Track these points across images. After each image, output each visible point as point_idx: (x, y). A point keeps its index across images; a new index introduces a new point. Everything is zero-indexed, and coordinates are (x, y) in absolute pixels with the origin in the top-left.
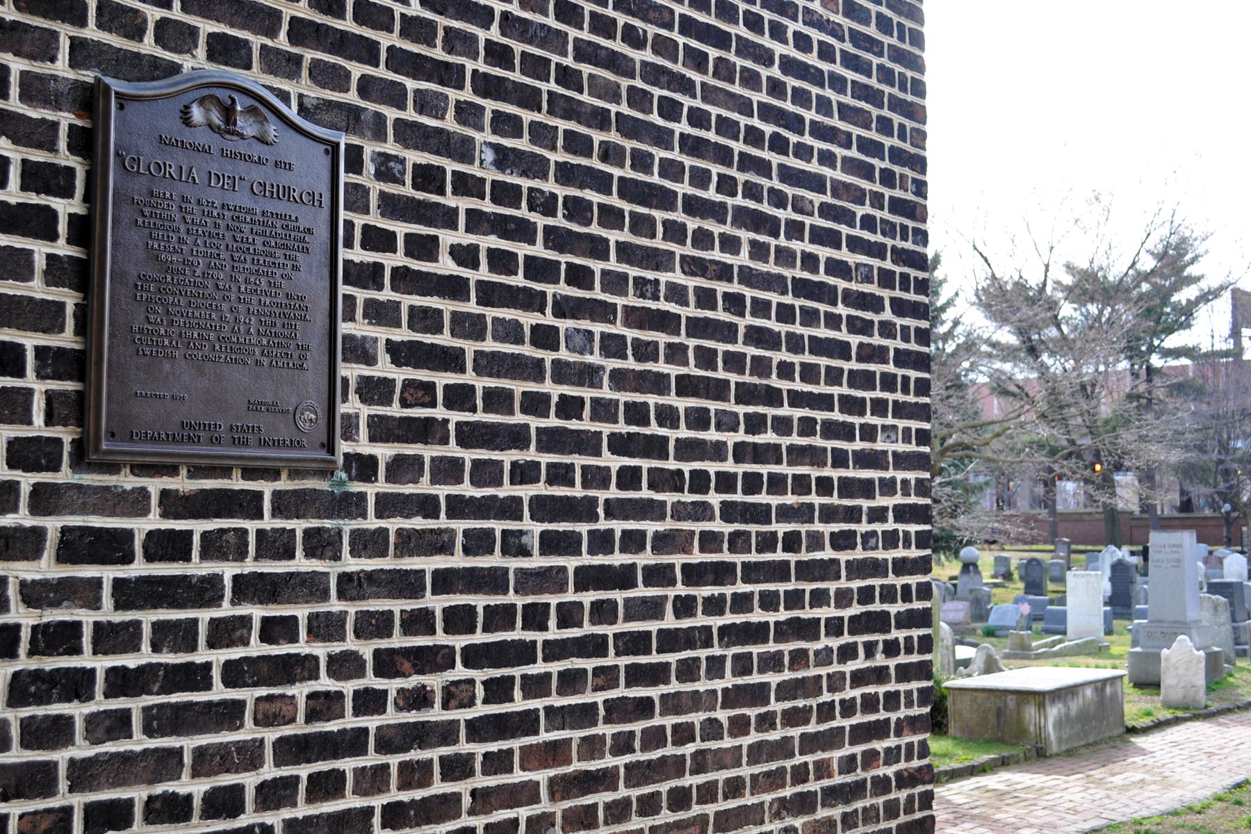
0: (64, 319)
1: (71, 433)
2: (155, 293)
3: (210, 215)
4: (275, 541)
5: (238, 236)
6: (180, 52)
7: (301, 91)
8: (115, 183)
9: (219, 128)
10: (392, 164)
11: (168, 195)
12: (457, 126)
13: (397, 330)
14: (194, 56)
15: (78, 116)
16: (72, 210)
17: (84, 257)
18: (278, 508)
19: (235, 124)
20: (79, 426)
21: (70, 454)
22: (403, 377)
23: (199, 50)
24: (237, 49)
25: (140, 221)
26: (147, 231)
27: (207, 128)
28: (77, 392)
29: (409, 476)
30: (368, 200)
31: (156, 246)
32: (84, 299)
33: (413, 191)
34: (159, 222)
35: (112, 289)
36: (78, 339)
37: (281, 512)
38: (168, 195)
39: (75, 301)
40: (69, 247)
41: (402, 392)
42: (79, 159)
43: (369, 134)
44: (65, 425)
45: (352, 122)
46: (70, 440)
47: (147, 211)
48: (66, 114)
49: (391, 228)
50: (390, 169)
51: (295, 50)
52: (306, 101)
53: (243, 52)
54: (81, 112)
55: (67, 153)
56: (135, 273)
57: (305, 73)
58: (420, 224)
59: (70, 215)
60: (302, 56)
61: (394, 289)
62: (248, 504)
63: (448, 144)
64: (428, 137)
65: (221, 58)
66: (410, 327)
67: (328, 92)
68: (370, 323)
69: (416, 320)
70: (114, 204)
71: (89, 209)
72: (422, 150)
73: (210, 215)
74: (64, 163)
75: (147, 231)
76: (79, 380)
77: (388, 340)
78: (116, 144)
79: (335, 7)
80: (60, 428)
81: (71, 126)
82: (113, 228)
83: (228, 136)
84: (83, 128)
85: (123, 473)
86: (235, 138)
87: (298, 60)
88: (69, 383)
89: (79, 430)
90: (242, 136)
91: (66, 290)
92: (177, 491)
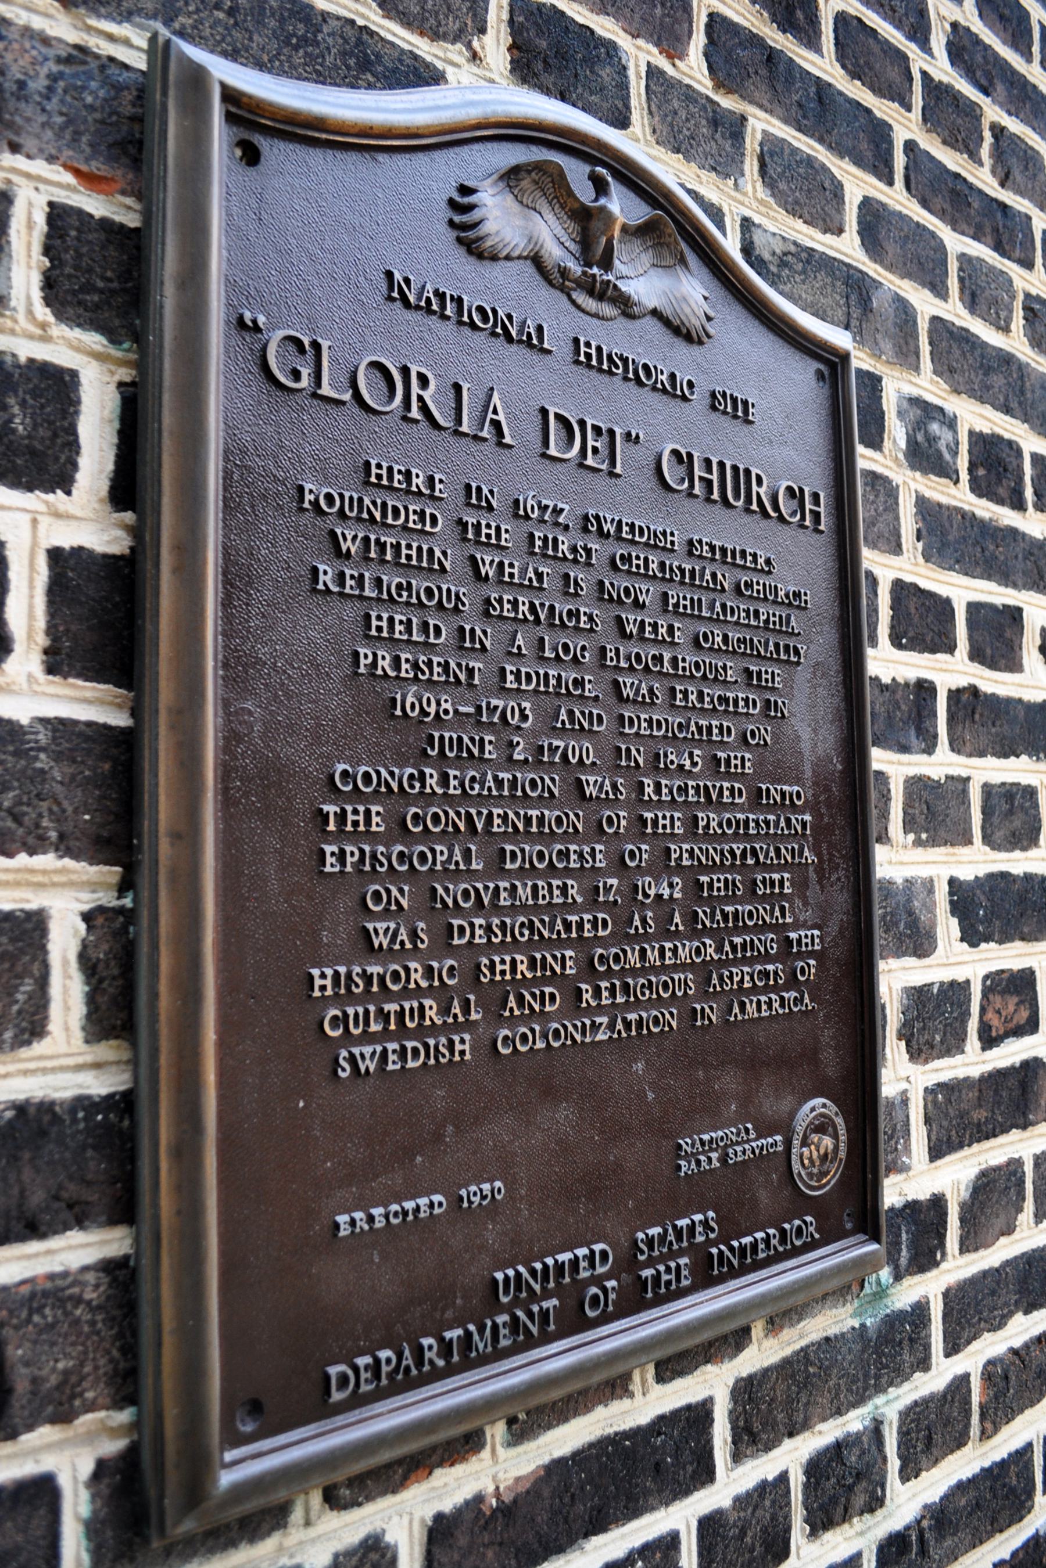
0: (43, 982)
1: (90, 1437)
2: (387, 840)
3: (549, 551)
4: (743, 1533)
5: (631, 617)
6: (436, 35)
7: (748, 213)
8: (229, 429)
9: (564, 272)
10: (935, 427)
11: (419, 482)
12: (1028, 350)
13: (963, 851)
14: (475, 57)
15: (89, 179)
16: (67, 538)
17: (120, 720)
18: (748, 1430)
19: (607, 264)
20: (118, 1403)
21: (93, 1529)
22: (983, 970)
23: (489, 39)
24: (591, 62)
25: (327, 578)
26: (351, 612)
27: (529, 268)
28: (110, 1267)
29: (1000, 1223)
30: (897, 518)
31: (385, 663)
32: (124, 886)
33: (972, 498)
34: (392, 580)
35: (228, 842)
36: (106, 1051)
37: (754, 1439)
38: (419, 482)
39: (87, 901)
40: (56, 685)
41: (983, 1010)
42: (95, 340)
43: (887, 346)
44: (63, 1417)
45: (856, 313)
46: (86, 1467)
47: (350, 541)
48: (39, 167)
49: (942, 591)
50: (932, 440)
51: (727, 102)
52: (758, 238)
53: (606, 73)
54: (96, 166)
55: (43, 313)
56: (314, 769)
57: (751, 166)
58: (989, 578)
59: (55, 555)
60: (743, 119)
61: (956, 746)
62: (676, 1457)
63: (1022, 392)
64: (988, 370)
65: (549, 80)
66: (987, 839)
67: (799, 224)
68: (918, 843)
69: (996, 820)
70: (229, 507)
71: (136, 532)
72: (982, 401)
73: (549, 551)
74: (26, 350)
75: (351, 612)
76: (113, 1222)
77: (952, 882)
78: (230, 283)
79: (800, 14)
80: (45, 1433)
81: (57, 214)
82: (226, 603)
83: (581, 298)
84: (105, 224)
85: (297, 1515)
86: (607, 309)
87: (736, 127)
88: (75, 1237)
89: (124, 1416)
90: (625, 305)
91: (47, 860)
92: (479, 1499)
